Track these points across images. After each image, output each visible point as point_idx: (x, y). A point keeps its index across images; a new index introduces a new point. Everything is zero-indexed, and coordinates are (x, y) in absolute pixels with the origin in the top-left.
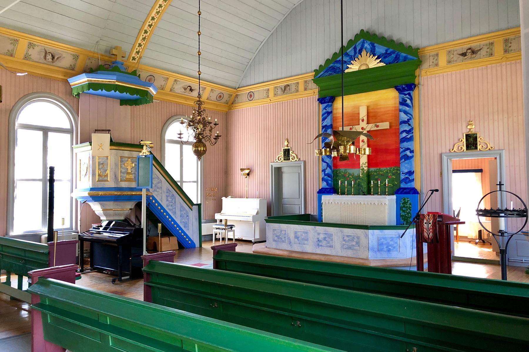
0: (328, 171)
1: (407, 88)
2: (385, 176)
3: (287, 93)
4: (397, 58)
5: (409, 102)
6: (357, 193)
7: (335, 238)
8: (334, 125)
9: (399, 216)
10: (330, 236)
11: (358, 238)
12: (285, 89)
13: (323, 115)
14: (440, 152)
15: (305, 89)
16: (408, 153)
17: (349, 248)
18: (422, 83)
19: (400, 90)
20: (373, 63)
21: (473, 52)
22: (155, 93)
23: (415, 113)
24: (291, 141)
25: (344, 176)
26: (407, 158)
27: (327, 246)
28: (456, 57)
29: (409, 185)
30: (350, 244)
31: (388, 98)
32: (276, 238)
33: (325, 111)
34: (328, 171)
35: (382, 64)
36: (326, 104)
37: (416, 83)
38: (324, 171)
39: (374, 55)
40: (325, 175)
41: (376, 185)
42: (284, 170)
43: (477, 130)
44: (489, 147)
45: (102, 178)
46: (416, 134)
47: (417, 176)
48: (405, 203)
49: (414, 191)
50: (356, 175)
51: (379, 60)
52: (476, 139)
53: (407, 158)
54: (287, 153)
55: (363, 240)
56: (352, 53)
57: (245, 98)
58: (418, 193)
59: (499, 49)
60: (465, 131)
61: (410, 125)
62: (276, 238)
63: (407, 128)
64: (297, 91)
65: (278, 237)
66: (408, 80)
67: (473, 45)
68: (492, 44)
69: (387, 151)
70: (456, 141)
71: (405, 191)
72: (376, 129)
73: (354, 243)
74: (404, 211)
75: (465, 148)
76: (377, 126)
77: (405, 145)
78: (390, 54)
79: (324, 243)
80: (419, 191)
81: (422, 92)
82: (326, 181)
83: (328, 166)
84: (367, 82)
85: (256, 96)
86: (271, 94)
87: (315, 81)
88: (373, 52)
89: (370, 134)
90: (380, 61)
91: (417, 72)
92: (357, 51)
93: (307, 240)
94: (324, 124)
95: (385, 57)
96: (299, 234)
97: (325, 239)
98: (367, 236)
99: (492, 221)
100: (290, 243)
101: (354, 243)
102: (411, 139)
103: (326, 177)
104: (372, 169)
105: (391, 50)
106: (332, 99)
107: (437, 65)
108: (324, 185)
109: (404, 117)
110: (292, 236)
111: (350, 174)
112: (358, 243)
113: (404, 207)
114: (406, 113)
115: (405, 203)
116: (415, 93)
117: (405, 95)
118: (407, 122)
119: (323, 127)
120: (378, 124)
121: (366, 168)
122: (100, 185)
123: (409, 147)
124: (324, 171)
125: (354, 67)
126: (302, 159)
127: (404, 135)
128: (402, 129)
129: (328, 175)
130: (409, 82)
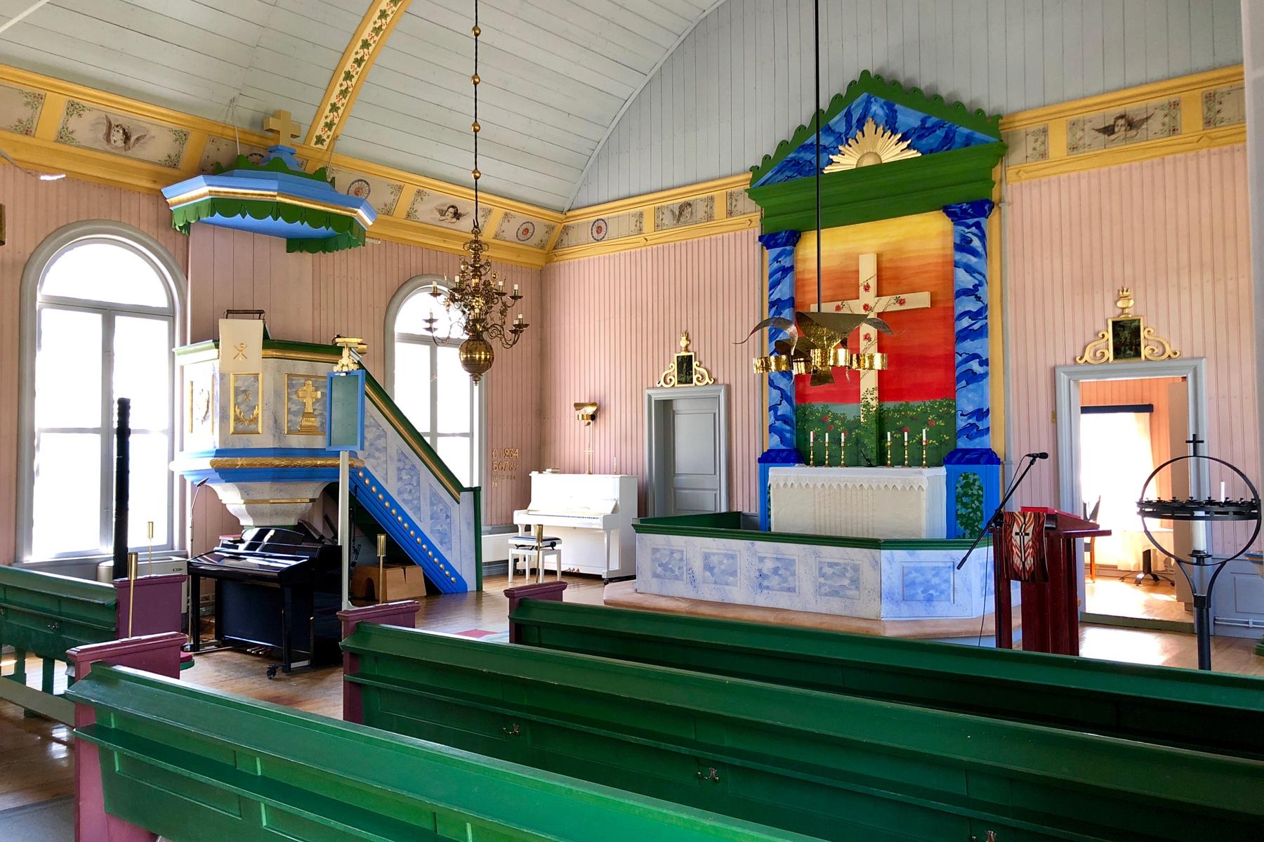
0: (784, 409)
1: (972, 211)
2: (920, 421)
3: (685, 223)
4: (948, 140)
5: (976, 243)
6: (854, 462)
7: (800, 569)
8: (798, 300)
9: (953, 516)
10: (789, 564)
11: (856, 569)
12: (680, 213)
13: (771, 276)
14: (1051, 363)
15: (730, 213)
16: (975, 365)
17: (835, 593)
18: (1008, 198)
19: (955, 215)
20: (892, 151)
21: (1131, 125)
22: (370, 223)
23: (992, 270)
24: (694, 336)
25: (823, 420)
26: (973, 377)
27: (781, 590)
28: (1089, 136)
29: (977, 444)
30: (837, 583)
31: (926, 234)
32: (659, 570)
33: (776, 265)
34: (784, 409)
35: (913, 154)
36: (778, 250)
37: (995, 198)
38: (773, 408)
39: (894, 132)
40: (777, 418)
41: (898, 443)
42: (679, 406)
43: (1140, 311)
44: (1169, 352)
45: (245, 425)
46: (994, 320)
47: (995, 421)
48: (968, 485)
49: (990, 458)
50: (850, 418)
51: (905, 144)
52: (1136, 332)
53: (973, 377)
54: (685, 366)
55: (868, 575)
56: (842, 128)
57: (585, 234)
58: (998, 462)
59: (1192, 116)
60: (1112, 314)
61: (978, 299)
62: (659, 570)
63: (973, 306)
64: (710, 217)
65: (664, 566)
66: (974, 192)
67: (1131, 108)
68: (1176, 104)
69: (924, 361)
70: (1090, 337)
71: (967, 457)
72: (898, 307)
73: (846, 582)
74: (965, 505)
75: (1110, 354)
76: (902, 302)
77: (969, 346)
78: (932, 130)
79: (774, 581)
80: (1001, 456)
81: (1008, 220)
82: (780, 433)
83: (784, 396)
84: (877, 195)
85: (612, 229)
86: (648, 224)
87: (753, 193)
88: (891, 125)
89: (884, 321)
90: (909, 147)
91: (996, 173)
92: (854, 121)
93: (734, 574)
94: (774, 297)
95: (920, 137)
96: (714, 559)
97: (776, 571)
98: (876, 564)
99: (1175, 527)
100: (693, 580)
101: (846, 582)
102: (982, 333)
103: (778, 423)
104: (889, 405)
105: (933, 120)
106: (794, 238)
107: (1044, 155)
108: (774, 442)
109: (965, 280)
110: (697, 565)
111: (835, 417)
112: (855, 582)
113: (965, 494)
114: (969, 269)
115: (968, 485)
116: (991, 224)
117: (969, 227)
118: (972, 292)
119: (772, 304)
120: (902, 296)
121: (874, 403)
122: (239, 443)
123: (978, 351)
124: (773, 408)
125: (846, 160)
126: (721, 381)
127: (966, 322)
128: (960, 309)
129: (785, 419)
130: (978, 195)
